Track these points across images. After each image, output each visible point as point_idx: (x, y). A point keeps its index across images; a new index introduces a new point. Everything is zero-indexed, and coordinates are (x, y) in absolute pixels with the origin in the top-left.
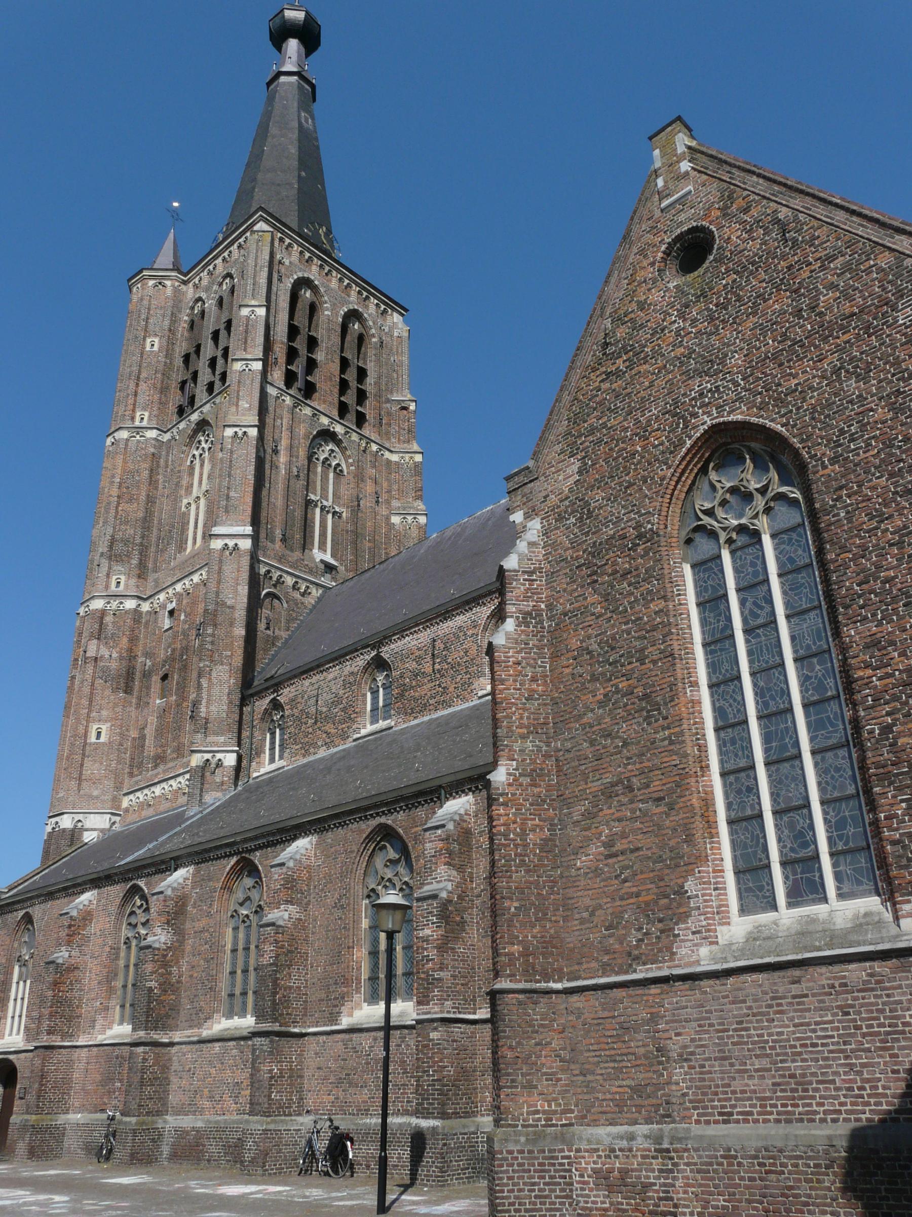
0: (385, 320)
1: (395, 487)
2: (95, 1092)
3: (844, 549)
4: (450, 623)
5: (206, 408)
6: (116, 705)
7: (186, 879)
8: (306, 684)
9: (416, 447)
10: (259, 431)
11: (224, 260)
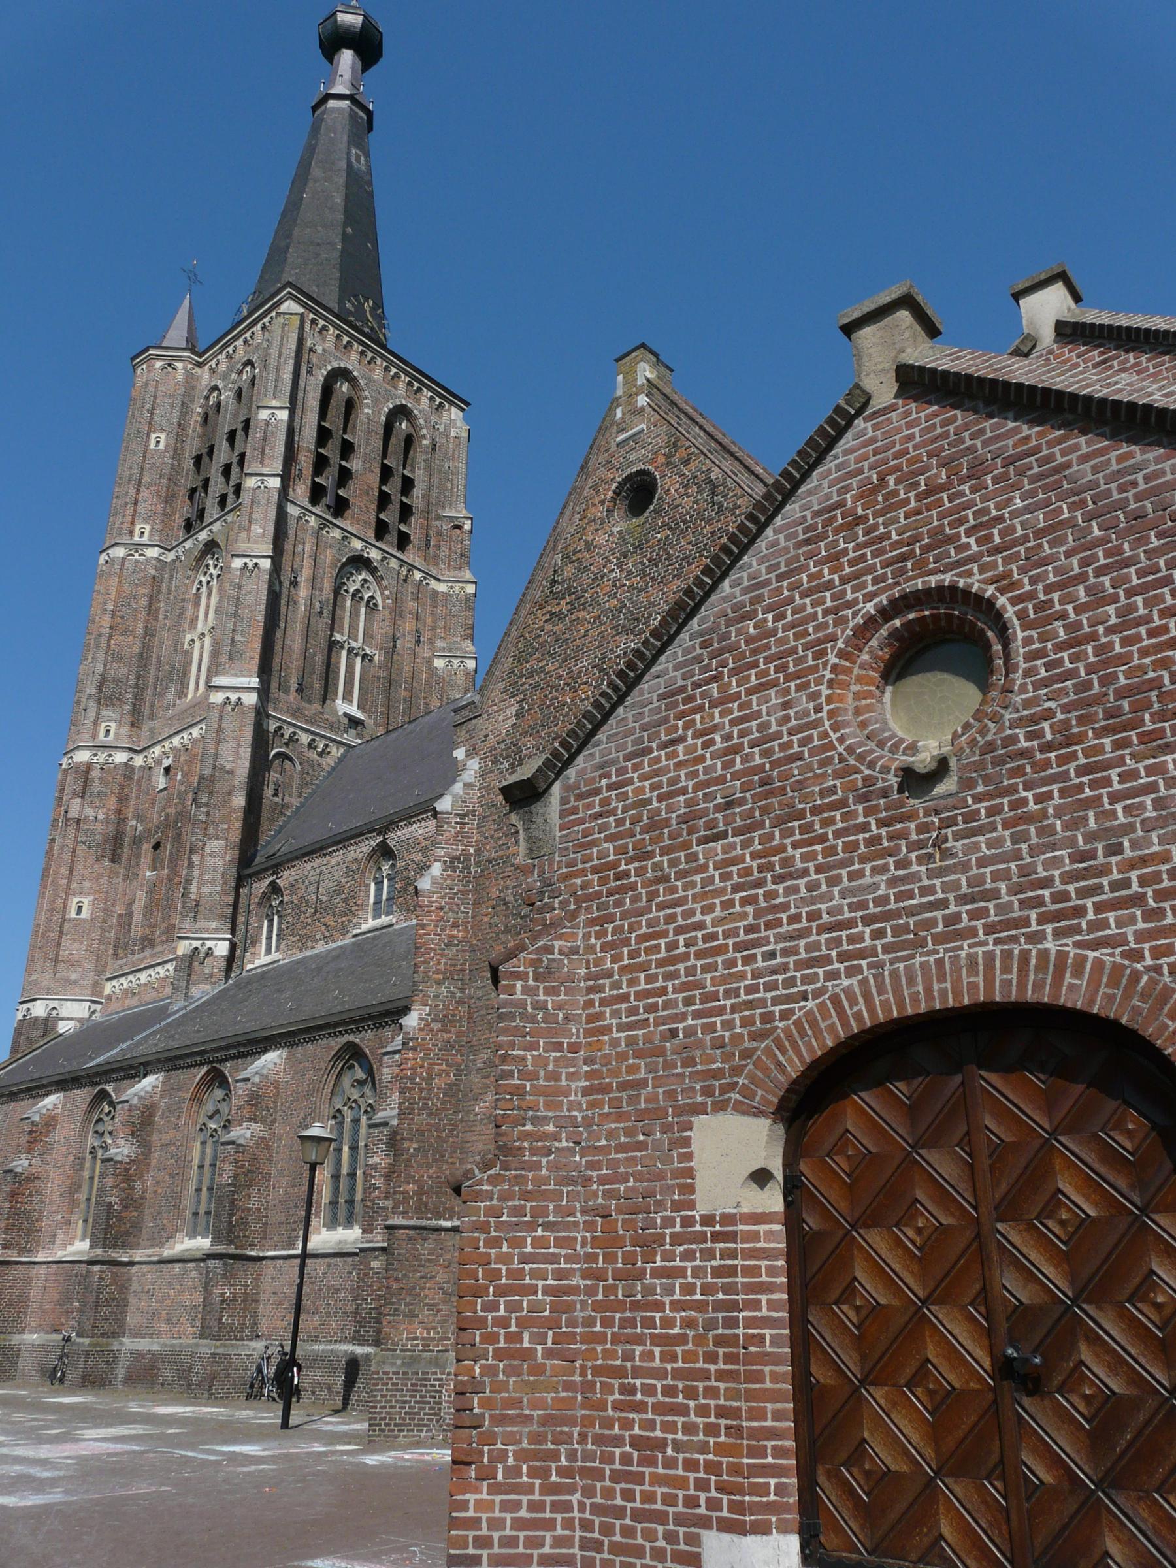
0: (440, 417)
1: (441, 623)
2: (53, 1311)
5: (216, 527)
6: (100, 875)
7: (154, 1087)
8: (308, 868)
9: (468, 576)
10: (273, 562)
11: (245, 341)
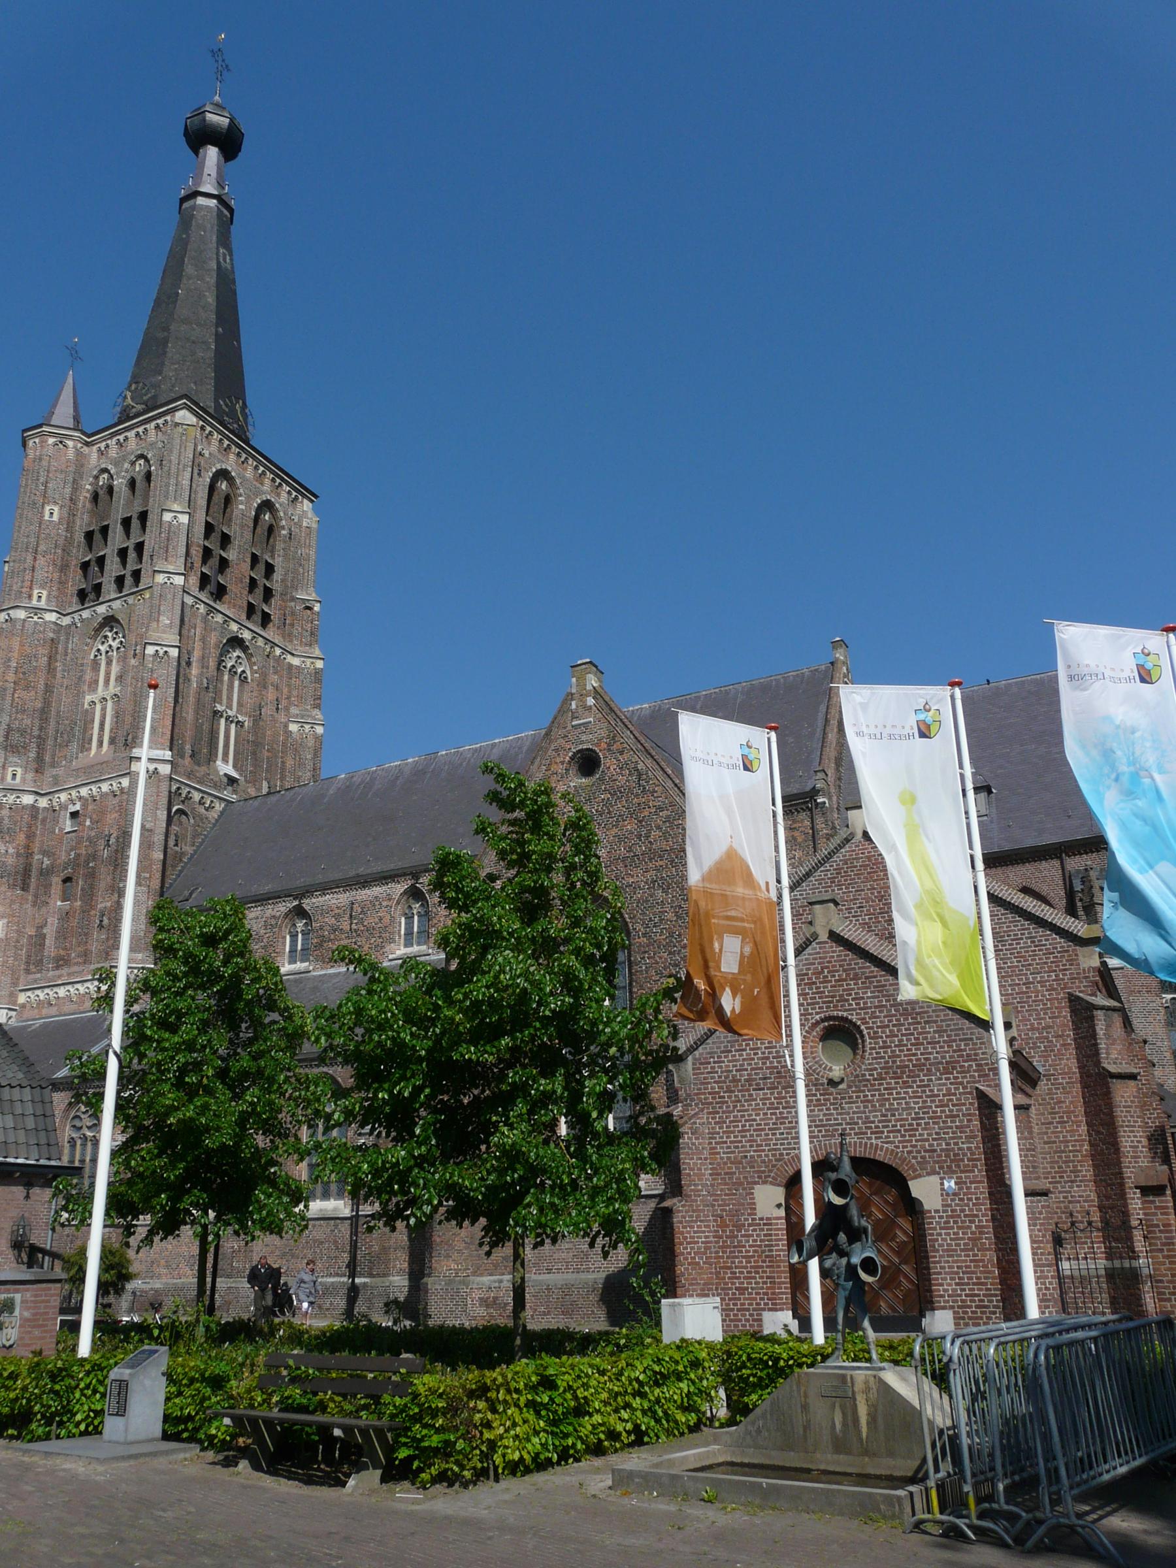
1: (295, 693)
3: (642, 988)
4: (367, 891)
6: (12, 902)
9: (317, 652)
11: (137, 435)
